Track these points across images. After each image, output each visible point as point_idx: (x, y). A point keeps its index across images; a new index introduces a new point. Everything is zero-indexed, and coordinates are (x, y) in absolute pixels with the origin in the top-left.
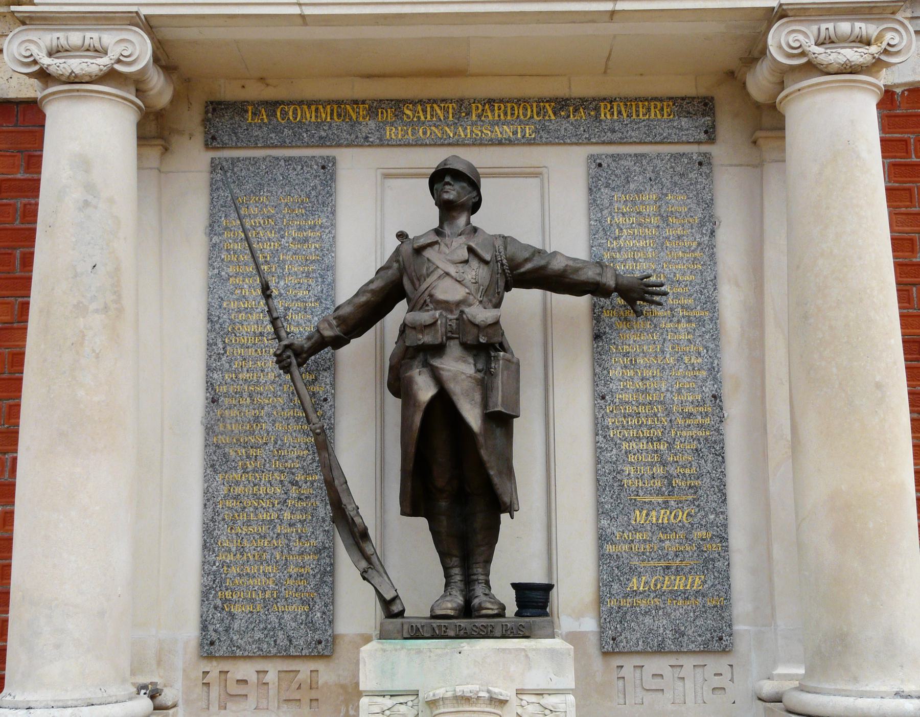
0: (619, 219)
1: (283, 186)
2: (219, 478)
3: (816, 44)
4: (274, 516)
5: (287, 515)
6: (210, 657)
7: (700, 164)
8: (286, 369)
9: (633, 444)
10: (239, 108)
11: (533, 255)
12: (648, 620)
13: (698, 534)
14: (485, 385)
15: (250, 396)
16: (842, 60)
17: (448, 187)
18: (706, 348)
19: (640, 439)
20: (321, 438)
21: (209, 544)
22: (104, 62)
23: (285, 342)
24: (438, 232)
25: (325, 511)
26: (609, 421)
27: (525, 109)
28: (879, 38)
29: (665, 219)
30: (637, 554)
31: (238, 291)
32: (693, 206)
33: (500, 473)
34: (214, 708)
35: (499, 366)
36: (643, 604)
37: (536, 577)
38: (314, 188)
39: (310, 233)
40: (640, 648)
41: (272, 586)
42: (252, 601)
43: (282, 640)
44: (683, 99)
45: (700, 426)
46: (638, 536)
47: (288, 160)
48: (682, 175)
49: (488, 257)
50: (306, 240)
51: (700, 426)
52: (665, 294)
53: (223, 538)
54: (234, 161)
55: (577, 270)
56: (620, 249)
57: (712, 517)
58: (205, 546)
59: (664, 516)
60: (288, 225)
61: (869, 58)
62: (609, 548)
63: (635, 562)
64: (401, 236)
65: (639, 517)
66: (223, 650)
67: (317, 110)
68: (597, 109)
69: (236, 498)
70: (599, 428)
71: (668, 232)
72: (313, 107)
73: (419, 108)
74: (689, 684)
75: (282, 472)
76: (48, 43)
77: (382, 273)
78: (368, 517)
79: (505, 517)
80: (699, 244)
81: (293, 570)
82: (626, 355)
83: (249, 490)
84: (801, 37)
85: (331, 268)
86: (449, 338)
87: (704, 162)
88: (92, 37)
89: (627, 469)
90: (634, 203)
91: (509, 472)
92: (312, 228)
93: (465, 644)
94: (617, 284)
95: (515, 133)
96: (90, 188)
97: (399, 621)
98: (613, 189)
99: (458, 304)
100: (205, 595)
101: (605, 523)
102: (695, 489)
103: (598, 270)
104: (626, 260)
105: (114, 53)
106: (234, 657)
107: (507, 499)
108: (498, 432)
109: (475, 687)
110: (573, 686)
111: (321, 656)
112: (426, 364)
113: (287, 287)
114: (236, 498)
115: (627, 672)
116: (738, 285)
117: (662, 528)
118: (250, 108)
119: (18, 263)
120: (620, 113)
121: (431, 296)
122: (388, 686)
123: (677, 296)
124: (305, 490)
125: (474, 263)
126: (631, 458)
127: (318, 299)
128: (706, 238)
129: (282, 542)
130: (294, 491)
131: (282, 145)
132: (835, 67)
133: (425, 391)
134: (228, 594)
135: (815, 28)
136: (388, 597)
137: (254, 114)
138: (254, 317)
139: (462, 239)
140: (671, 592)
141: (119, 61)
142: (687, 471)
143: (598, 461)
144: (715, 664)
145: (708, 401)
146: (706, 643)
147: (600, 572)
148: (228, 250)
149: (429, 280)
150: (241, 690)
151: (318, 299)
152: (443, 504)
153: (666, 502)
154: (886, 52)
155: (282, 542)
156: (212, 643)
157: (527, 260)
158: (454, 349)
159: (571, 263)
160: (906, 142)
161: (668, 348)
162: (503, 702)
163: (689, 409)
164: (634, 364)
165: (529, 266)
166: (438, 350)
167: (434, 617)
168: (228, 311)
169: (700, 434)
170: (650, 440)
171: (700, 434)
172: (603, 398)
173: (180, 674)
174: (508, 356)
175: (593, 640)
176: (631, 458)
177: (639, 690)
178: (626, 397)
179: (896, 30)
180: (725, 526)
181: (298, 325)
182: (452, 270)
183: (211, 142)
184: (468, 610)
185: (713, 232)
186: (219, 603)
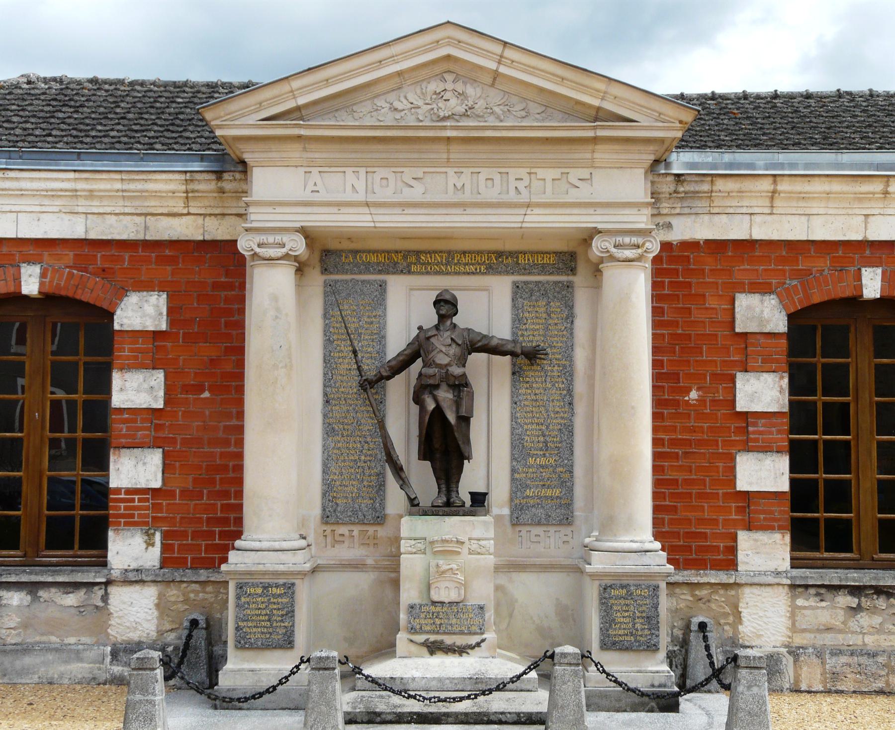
0: (526, 315)
1: (360, 295)
2: (330, 439)
3: (614, 247)
4: (357, 458)
5: (363, 458)
6: (327, 523)
7: (568, 287)
8: (365, 390)
9: (529, 426)
10: (338, 253)
11: (482, 338)
12: (534, 510)
13: (559, 469)
14: (458, 403)
15: (345, 400)
16: (624, 256)
17: (442, 308)
18: (567, 380)
19: (533, 424)
20: (381, 424)
21: (325, 470)
22: (284, 251)
23: (364, 378)
24: (437, 327)
25: (382, 456)
26: (518, 415)
27: (481, 257)
28: (644, 244)
29: (549, 315)
30: (530, 479)
31: (338, 348)
32: (564, 308)
33: (464, 443)
34: (329, 547)
35: (464, 394)
36: (532, 502)
37: (481, 489)
38: (376, 296)
39: (374, 319)
40: (530, 522)
41: (356, 491)
42: (346, 498)
43: (361, 517)
44: (561, 253)
45: (562, 418)
46: (531, 470)
47: (363, 282)
48: (558, 293)
49: (460, 342)
50: (372, 323)
51: (562, 418)
52: (546, 354)
53: (332, 468)
54: (336, 282)
55: (503, 345)
56: (526, 330)
57: (566, 461)
58: (324, 472)
59: (543, 461)
60: (363, 315)
61: (637, 255)
62: (517, 476)
63: (528, 482)
64: (420, 328)
65: (531, 461)
66: (333, 520)
67: (377, 256)
68: (517, 258)
69: (339, 449)
70: (513, 418)
71: (550, 321)
72: (375, 255)
73: (428, 256)
74: (552, 540)
75: (360, 437)
76: (258, 241)
77: (410, 346)
78: (402, 460)
79: (466, 462)
80: (566, 328)
81: (365, 483)
82: (527, 382)
83: (345, 445)
84: (607, 244)
85: (384, 337)
86: (441, 381)
87: (569, 286)
88: (278, 238)
89: (526, 438)
90: (534, 306)
91: (468, 441)
92: (375, 316)
93: (447, 518)
94: (522, 351)
95: (476, 269)
96: (278, 309)
97: (418, 508)
98: (524, 299)
99: (446, 365)
100: (324, 495)
101: (515, 463)
102: (558, 448)
103: (513, 345)
104: (529, 335)
105: (288, 247)
106: (337, 523)
107: (467, 455)
108: (463, 424)
109: (451, 536)
110: (493, 536)
111: (379, 524)
112: (431, 393)
113: (362, 346)
114: (339, 449)
115: (523, 533)
116: (584, 348)
117: (542, 466)
118: (344, 254)
119: (223, 325)
120: (529, 260)
121: (434, 361)
122: (413, 535)
123: (553, 354)
124: (372, 445)
125: (454, 346)
126: (528, 433)
127: (378, 353)
128: (569, 325)
129: (360, 470)
130: (366, 447)
131: (360, 273)
132: (621, 259)
133: (431, 406)
134: (335, 494)
135: (614, 239)
136: (412, 497)
137: (346, 257)
138: (347, 361)
139: (448, 333)
140: (545, 496)
141: (290, 250)
142: (555, 440)
143: (512, 434)
144: (564, 530)
145: (566, 405)
146: (560, 521)
147: (511, 487)
148: (333, 327)
149: (433, 354)
150: (341, 539)
151: (378, 353)
152: (438, 456)
153: (544, 454)
154: (645, 251)
155: (360, 470)
156: (328, 517)
157: (479, 341)
158: (444, 386)
159: (500, 342)
160: (677, 270)
161: (548, 379)
162: (463, 543)
163: (557, 409)
164: (531, 387)
165: (480, 344)
166: (437, 387)
167: (433, 506)
168: (334, 358)
169: (562, 421)
170: (538, 424)
171: (562, 421)
172: (516, 403)
173: (312, 531)
174: (468, 389)
175: (508, 519)
176: (528, 433)
177: (529, 542)
178: (526, 403)
179: (651, 241)
180: (572, 466)
181: (368, 365)
182: (444, 349)
183: (325, 271)
184: (448, 504)
185: (572, 321)
186: (331, 498)
